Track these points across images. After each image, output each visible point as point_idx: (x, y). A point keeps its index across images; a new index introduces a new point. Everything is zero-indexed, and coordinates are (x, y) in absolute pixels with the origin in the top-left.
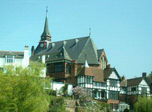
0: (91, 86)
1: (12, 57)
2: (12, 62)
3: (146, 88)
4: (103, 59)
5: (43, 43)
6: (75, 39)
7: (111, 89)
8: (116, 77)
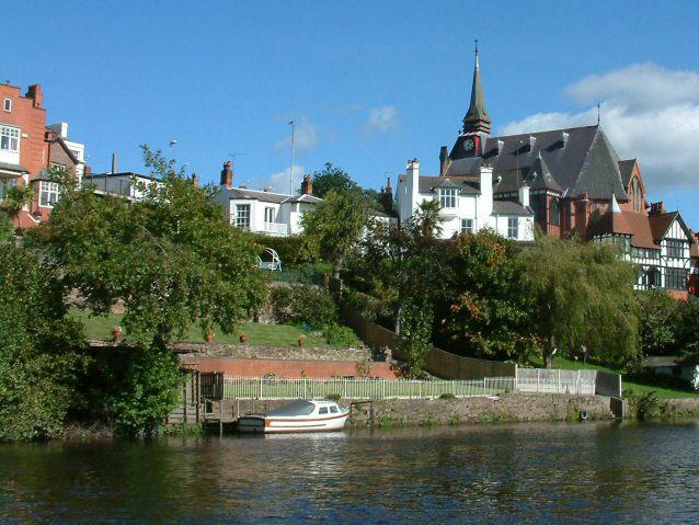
1: (453, 194)
2: (453, 206)
4: (635, 186)
5: (472, 138)
6: (528, 136)
7: (670, 265)
8: (681, 235)
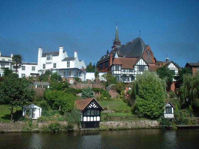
0: (120, 72)
3: (174, 70)
